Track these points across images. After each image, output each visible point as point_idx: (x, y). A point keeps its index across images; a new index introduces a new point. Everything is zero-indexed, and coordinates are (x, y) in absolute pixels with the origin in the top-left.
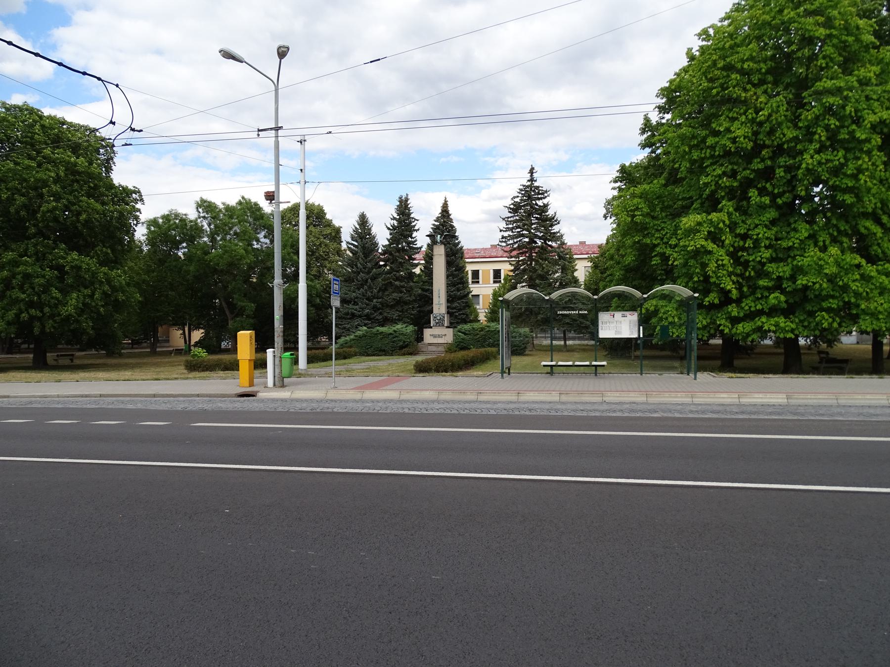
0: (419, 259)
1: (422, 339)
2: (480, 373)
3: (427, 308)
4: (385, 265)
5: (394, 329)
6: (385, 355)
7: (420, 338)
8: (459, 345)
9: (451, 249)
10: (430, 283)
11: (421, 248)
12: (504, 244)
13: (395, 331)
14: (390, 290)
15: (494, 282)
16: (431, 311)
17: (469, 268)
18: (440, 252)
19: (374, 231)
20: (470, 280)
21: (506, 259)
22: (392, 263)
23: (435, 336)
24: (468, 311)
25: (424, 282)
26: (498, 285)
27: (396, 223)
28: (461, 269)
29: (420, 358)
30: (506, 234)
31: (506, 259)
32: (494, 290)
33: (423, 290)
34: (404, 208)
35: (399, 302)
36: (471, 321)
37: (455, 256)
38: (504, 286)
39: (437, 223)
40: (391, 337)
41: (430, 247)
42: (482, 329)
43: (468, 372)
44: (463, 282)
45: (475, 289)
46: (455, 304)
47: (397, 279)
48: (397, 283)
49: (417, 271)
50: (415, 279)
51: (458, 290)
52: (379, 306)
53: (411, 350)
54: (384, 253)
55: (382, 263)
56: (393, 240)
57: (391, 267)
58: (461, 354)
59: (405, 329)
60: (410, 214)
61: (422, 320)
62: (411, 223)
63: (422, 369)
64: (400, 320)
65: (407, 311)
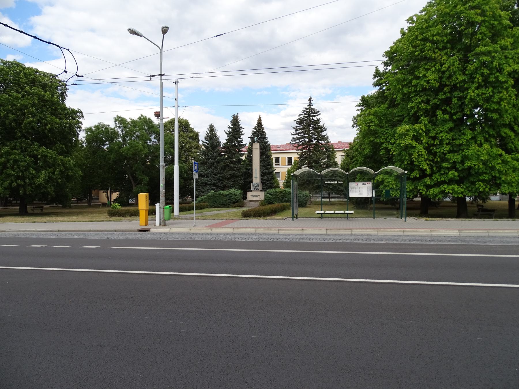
0: (244, 151)
1: (246, 198)
2: (280, 218)
3: (249, 180)
4: (224, 155)
5: (230, 192)
6: (225, 207)
7: (245, 197)
8: (268, 201)
9: (263, 145)
10: (251, 165)
11: (245, 145)
12: (294, 142)
13: (230, 193)
14: (228, 169)
15: (288, 164)
16: (252, 182)
17: (274, 156)
18: (256, 147)
19: (218, 135)
20: (274, 163)
21: (295, 151)
22: (228, 154)
23: (253, 196)
24: (273, 181)
25: (247, 165)
26: (290, 166)
27: (231, 130)
28: (269, 157)
29: (245, 209)
30: (295, 137)
31: (295, 151)
32: (288, 169)
33: (247, 169)
34: (235, 122)
35: (233, 176)
36: (275, 187)
37: (265, 149)
38: (294, 167)
39: (255, 130)
40: (228, 196)
41: (251, 144)
42: (281, 192)
43: (273, 217)
44: (270, 165)
45: (277, 169)
46: (266, 178)
47: (232, 163)
48: (232, 165)
49: (243, 158)
50: (242, 163)
51: (267, 169)
52: (221, 178)
53: (240, 204)
54: (224, 147)
55: (223, 153)
56: (229, 140)
57: (228, 156)
58: (269, 207)
59: (236, 192)
60: (239, 125)
61: (246, 187)
62: (239, 130)
63: (246, 215)
64: (233, 186)
65: (237, 181)
